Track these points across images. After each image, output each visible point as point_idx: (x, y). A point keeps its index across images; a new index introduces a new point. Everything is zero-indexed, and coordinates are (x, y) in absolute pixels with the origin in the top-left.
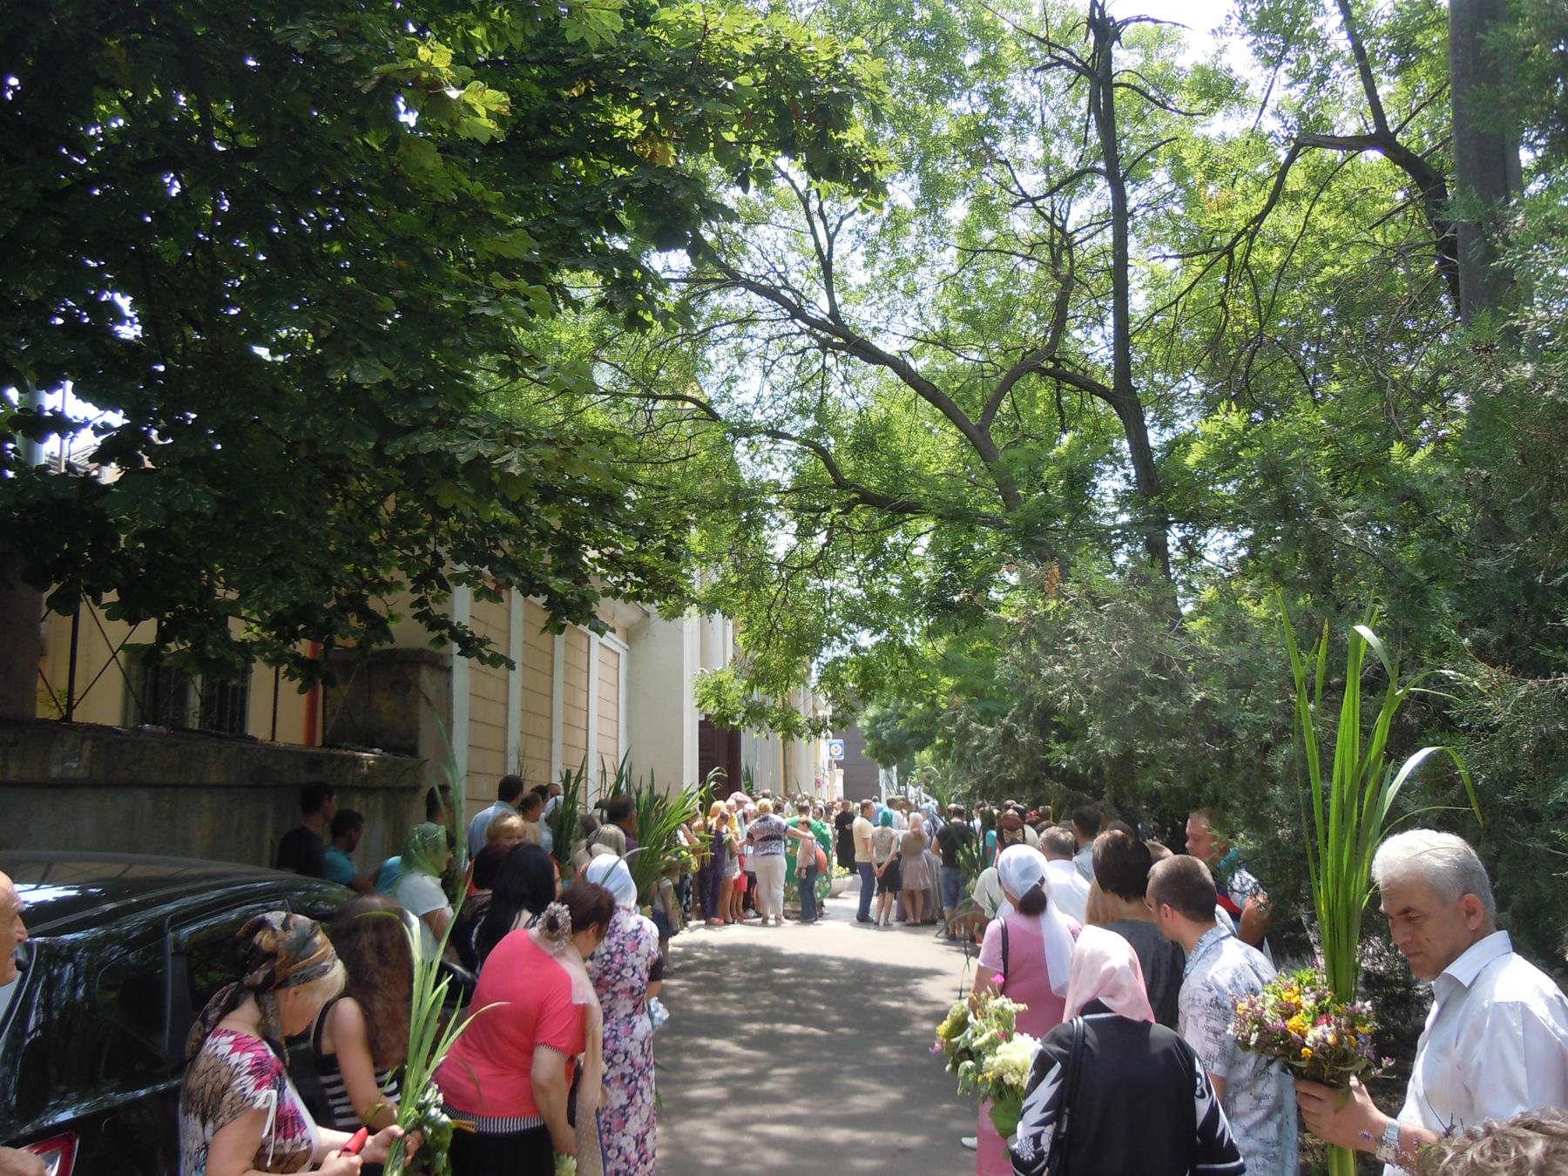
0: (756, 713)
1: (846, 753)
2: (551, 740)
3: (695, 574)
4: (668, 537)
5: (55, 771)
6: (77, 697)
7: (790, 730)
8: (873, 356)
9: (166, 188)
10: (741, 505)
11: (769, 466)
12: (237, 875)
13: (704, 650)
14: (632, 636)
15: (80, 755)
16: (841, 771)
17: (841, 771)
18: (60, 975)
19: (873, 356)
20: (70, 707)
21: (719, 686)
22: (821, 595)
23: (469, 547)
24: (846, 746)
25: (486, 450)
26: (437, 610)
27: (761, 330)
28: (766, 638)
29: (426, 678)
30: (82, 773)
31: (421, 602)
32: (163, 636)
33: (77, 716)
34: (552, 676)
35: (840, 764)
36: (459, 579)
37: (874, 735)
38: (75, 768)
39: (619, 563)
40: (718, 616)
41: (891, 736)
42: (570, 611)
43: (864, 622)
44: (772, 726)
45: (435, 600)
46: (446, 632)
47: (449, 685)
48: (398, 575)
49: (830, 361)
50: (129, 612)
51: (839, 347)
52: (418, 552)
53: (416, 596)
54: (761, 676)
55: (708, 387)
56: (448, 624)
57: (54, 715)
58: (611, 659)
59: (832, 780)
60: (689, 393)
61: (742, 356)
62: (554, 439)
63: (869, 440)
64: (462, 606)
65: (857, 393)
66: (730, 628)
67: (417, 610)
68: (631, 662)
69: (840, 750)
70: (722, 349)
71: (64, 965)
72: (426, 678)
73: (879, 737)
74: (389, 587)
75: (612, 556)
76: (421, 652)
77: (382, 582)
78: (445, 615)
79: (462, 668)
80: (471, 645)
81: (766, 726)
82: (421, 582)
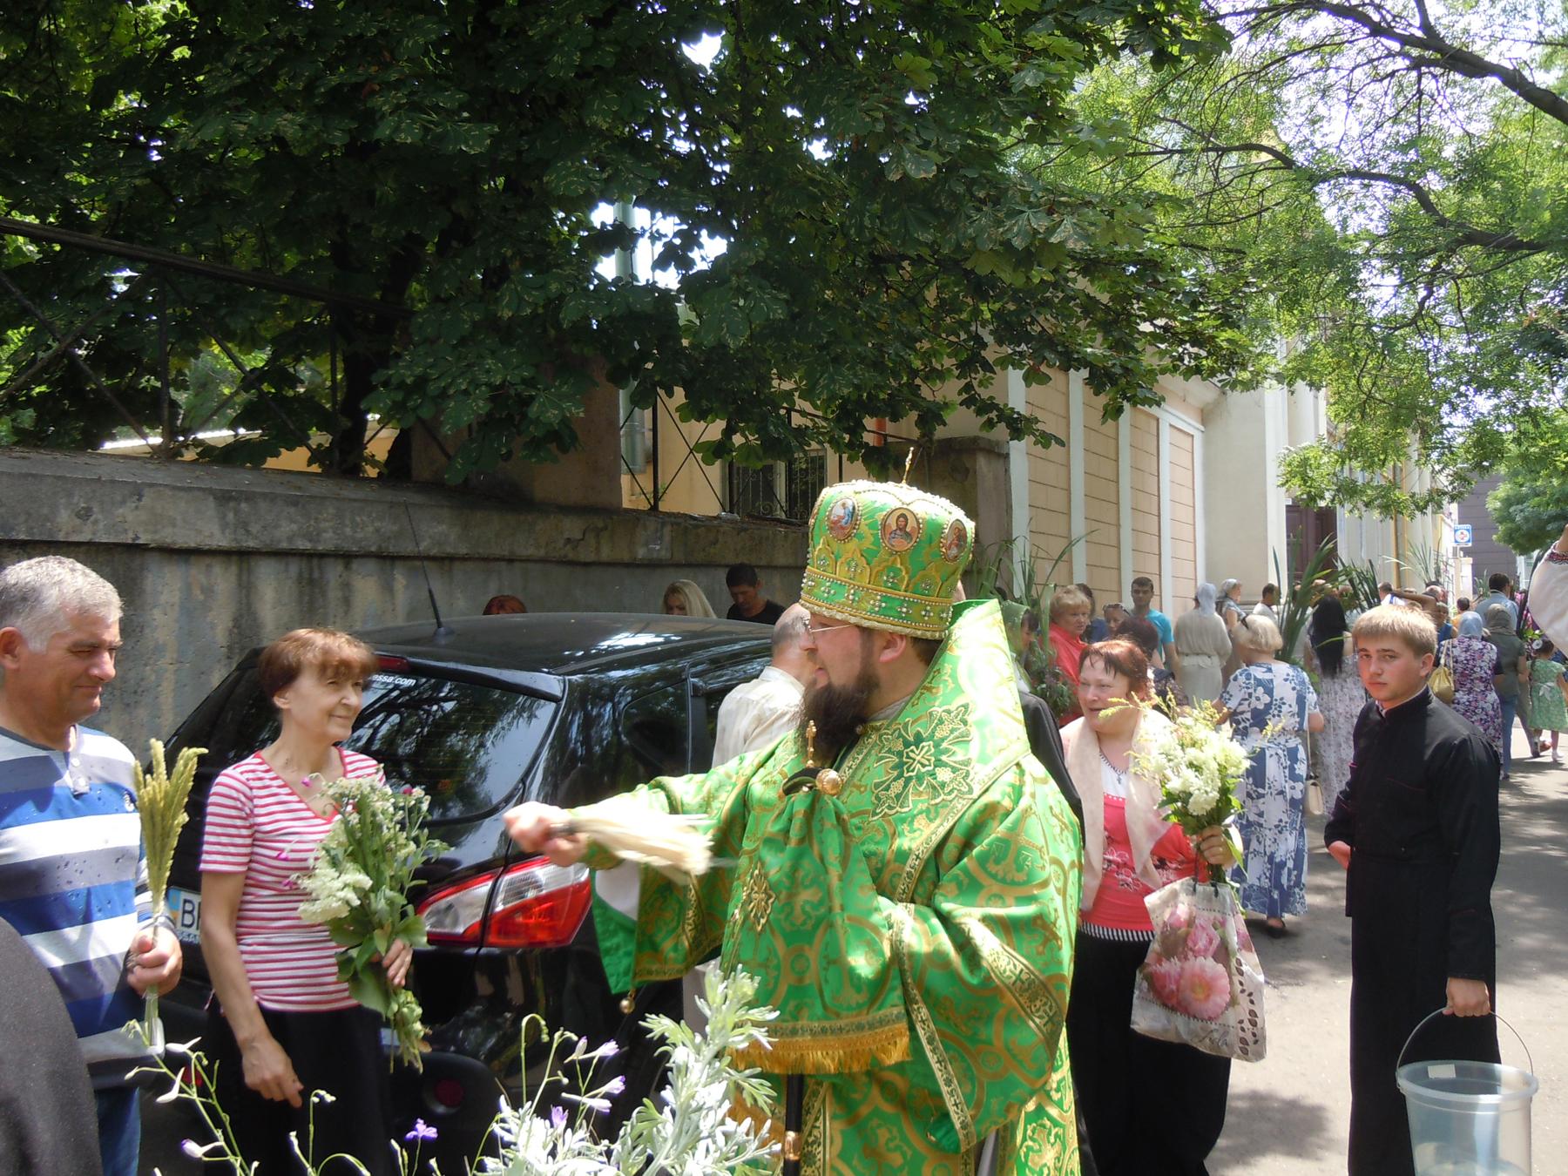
0: (1348, 490)
1: (1474, 539)
2: (1118, 526)
3: (1277, 346)
4: (1226, 302)
5: (641, 553)
6: (661, 491)
7: (1390, 508)
8: (1473, 66)
9: (183, 59)
10: (1333, 257)
11: (1358, 213)
12: (720, 633)
13: (1291, 421)
14: (1206, 416)
15: (661, 538)
16: (1470, 560)
17: (1470, 560)
18: (600, 715)
19: (1473, 66)
20: (657, 498)
21: (1305, 462)
22: (1421, 355)
23: (1009, 326)
24: (1475, 530)
25: (1041, 223)
26: (984, 393)
27: (1345, 60)
28: (1362, 408)
29: (982, 464)
30: (665, 555)
31: (968, 387)
32: (729, 432)
33: (663, 507)
34: (1117, 461)
35: (1467, 552)
36: (1004, 362)
37: (1505, 517)
38: (659, 550)
39: (1175, 334)
40: (1300, 385)
41: (1526, 519)
42: (1122, 387)
43: (1482, 385)
44: (1367, 505)
45: (981, 384)
46: (994, 414)
47: (1007, 471)
48: (949, 362)
49: (1429, 84)
50: (696, 410)
51: (1435, 63)
52: (963, 336)
53: (963, 382)
54: (1354, 449)
55: (1288, 132)
56: (995, 406)
57: (644, 505)
58: (1186, 442)
59: (1458, 570)
60: (1265, 142)
61: (1324, 93)
62: (1112, 206)
63: (1476, 169)
64: (1015, 391)
65: (1467, 115)
66: (1322, 403)
67: (965, 396)
68: (1208, 443)
69: (1468, 536)
70: (1301, 86)
71: (605, 705)
72: (982, 464)
73: (1513, 520)
74: (941, 375)
75: (1166, 328)
76: (975, 440)
77: (934, 370)
78: (991, 398)
79: (1019, 451)
80: (1019, 426)
81: (1360, 504)
82: (966, 367)
